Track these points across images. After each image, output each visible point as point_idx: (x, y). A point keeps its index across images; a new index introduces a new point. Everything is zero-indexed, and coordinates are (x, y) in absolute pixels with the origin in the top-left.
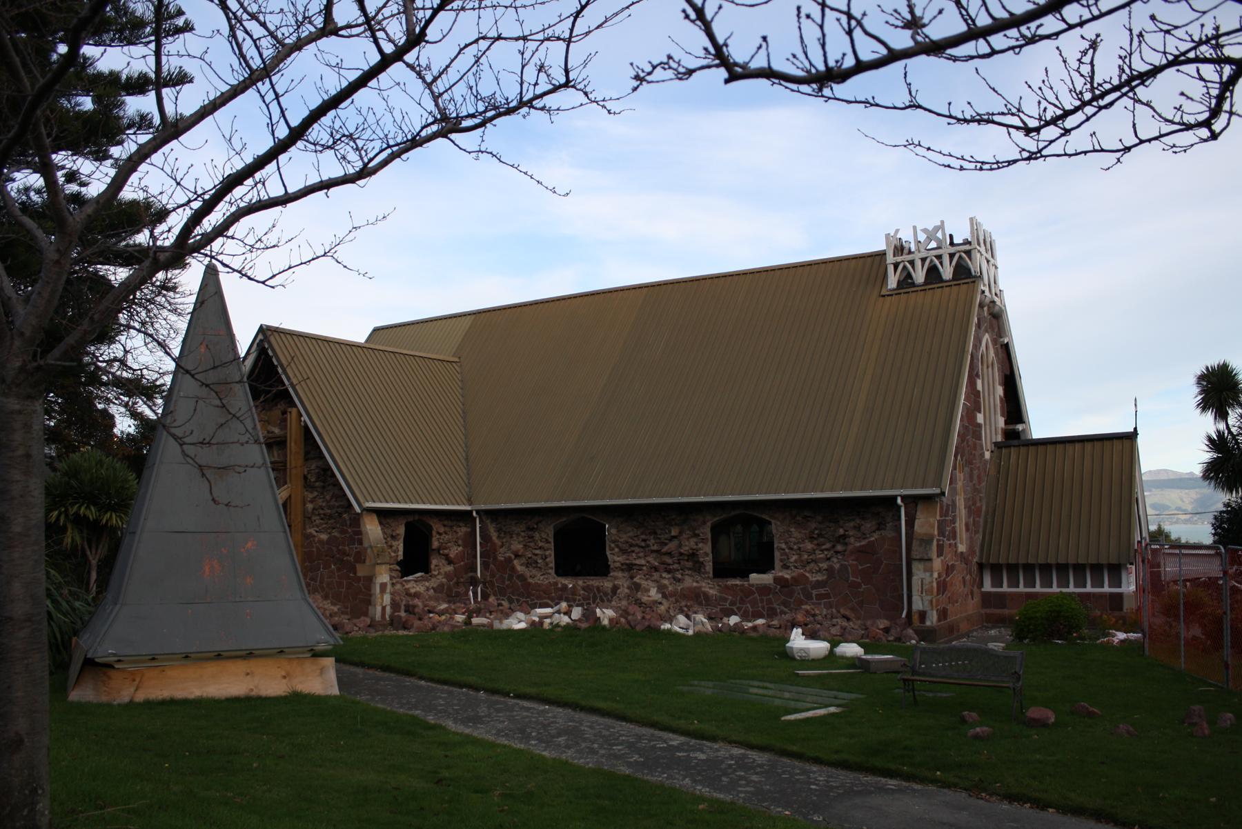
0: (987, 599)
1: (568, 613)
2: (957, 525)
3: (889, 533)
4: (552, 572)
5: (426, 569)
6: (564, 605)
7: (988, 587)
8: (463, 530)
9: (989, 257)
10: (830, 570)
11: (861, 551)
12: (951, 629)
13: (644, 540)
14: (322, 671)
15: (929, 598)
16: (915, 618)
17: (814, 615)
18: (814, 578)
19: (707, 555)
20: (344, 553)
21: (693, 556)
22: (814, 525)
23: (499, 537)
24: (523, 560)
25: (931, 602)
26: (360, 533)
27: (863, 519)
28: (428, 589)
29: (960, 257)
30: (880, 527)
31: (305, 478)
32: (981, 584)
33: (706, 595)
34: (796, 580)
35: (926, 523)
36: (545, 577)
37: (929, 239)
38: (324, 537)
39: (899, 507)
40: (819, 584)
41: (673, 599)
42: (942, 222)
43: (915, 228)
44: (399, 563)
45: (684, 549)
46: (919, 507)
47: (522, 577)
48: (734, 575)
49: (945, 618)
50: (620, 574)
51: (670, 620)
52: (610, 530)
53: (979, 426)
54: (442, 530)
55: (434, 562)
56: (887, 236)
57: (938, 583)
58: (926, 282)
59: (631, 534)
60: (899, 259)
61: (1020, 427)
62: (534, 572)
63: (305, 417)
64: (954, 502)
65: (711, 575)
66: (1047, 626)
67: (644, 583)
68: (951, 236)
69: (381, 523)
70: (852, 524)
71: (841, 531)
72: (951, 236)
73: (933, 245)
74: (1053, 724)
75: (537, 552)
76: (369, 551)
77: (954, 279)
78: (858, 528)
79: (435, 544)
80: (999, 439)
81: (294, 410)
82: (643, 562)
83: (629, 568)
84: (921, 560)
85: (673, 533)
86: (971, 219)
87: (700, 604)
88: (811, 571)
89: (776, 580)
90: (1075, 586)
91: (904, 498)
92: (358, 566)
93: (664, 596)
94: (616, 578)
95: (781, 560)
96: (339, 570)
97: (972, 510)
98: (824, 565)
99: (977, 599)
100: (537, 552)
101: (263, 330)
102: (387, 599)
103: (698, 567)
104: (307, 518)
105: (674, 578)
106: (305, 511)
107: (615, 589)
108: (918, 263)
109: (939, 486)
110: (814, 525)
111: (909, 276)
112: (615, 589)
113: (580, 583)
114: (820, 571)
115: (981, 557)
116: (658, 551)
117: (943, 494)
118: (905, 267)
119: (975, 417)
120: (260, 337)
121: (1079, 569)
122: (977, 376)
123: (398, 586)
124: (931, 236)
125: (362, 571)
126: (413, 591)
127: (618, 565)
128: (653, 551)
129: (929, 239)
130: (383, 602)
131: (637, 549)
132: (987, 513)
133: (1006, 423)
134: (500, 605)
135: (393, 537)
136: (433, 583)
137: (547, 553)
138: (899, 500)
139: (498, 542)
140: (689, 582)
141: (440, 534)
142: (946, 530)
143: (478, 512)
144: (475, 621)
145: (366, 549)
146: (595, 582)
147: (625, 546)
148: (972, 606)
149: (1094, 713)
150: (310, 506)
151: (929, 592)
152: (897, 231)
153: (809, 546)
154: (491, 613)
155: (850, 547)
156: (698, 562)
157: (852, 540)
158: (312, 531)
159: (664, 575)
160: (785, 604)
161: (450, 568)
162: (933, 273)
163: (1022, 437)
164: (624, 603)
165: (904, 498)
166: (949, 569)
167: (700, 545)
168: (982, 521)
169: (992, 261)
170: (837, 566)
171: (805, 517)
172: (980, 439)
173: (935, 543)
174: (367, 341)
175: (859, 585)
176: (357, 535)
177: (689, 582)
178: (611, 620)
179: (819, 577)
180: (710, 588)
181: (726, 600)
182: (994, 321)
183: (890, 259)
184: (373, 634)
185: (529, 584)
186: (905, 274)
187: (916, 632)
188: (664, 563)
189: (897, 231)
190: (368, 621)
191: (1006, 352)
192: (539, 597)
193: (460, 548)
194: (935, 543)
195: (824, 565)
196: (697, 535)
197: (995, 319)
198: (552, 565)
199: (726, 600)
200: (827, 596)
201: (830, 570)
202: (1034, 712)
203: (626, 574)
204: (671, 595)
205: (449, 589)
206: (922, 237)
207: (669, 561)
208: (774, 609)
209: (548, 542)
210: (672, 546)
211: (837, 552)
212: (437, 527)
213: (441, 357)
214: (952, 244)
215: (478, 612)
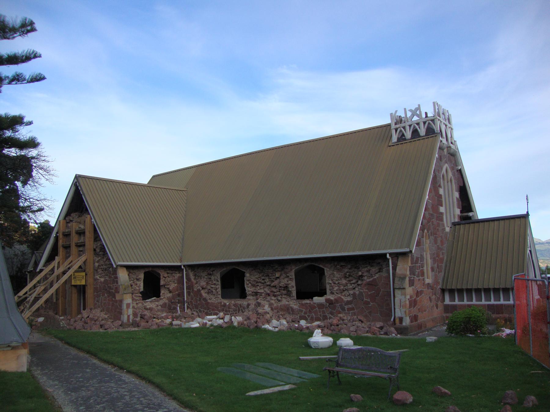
0: (448, 309)
1: (223, 318)
2: (425, 268)
3: (384, 274)
4: (220, 296)
5: (158, 295)
6: (221, 314)
7: (447, 301)
8: (177, 275)
9: (447, 124)
10: (354, 294)
11: (369, 284)
12: (420, 327)
13: (263, 280)
14: (18, 358)
15: (404, 310)
16: (397, 321)
17: (343, 320)
18: (346, 299)
19: (293, 287)
20: (110, 288)
21: (286, 287)
22: (346, 270)
23: (195, 279)
24: (206, 291)
25: (405, 312)
26: (117, 278)
27: (372, 266)
28: (157, 306)
29: (429, 123)
30: (380, 270)
31: (95, 250)
32: (444, 300)
33: (292, 308)
34: (337, 301)
35: (403, 267)
36: (216, 299)
37: (413, 116)
38: (102, 280)
39: (389, 259)
40: (349, 303)
41: (276, 311)
42: (419, 105)
43: (405, 109)
44: (141, 293)
45: (282, 284)
47: (205, 299)
48: (308, 298)
49: (416, 320)
50: (251, 297)
51: (268, 322)
52: (328, 272)
53: (442, 213)
54: (166, 275)
55: (162, 292)
56: (391, 114)
57: (410, 302)
59: (257, 276)
60: (397, 126)
61: (471, 214)
62: (212, 296)
63: (93, 220)
64: (422, 256)
65: (295, 298)
66: (465, 327)
67: (263, 302)
68: (426, 113)
69: (127, 271)
70: (366, 269)
71: (360, 273)
72: (426, 113)
73: (415, 118)
74: (411, 404)
75: (213, 286)
76: (121, 287)
78: (368, 271)
79: (162, 283)
80: (457, 220)
81: (89, 216)
82: (262, 291)
83: (256, 294)
84: (399, 289)
85: (277, 276)
86: (434, 103)
87: (289, 313)
88: (345, 295)
89: (327, 300)
90: (495, 301)
91: (391, 254)
92: (116, 294)
93: (272, 309)
94: (249, 300)
95: (330, 290)
96: (108, 297)
97: (436, 258)
98: (351, 292)
99: (441, 308)
100: (213, 286)
101: (77, 177)
102: (130, 311)
103: (289, 294)
104: (96, 270)
105: (277, 299)
106: (94, 266)
107: (248, 305)
108: (408, 128)
109: (408, 246)
110: (346, 270)
112: (248, 305)
113: (233, 302)
114: (349, 295)
115: (443, 285)
116: (270, 285)
117: (411, 251)
118: (401, 131)
119: (438, 209)
120: (76, 180)
121: (496, 291)
122: (440, 186)
123: (140, 305)
124: (414, 113)
125: (118, 297)
126: (148, 307)
127: (250, 293)
128: (267, 285)
129: (413, 116)
130: (128, 314)
131: (260, 284)
132: (447, 261)
133: (461, 212)
134: (193, 314)
135: (138, 280)
136: (161, 302)
137: (217, 287)
139: (194, 282)
140: (284, 302)
141: (165, 278)
142: (417, 271)
143: (184, 266)
144: (175, 322)
145: (119, 286)
146: (240, 302)
147: (254, 283)
148: (437, 313)
149: (445, 393)
150: (97, 264)
151: (404, 306)
152: (396, 111)
153: (344, 281)
154: (185, 318)
155: (364, 282)
156: (289, 291)
157: (365, 278)
158: (98, 277)
159: (273, 298)
160: (331, 313)
161: (170, 295)
162: (415, 133)
163: (473, 219)
164: (250, 313)
165: (390, 254)
166: (418, 294)
167: (290, 282)
168: (444, 265)
169: (449, 125)
170: (357, 293)
171: (341, 266)
172: (442, 220)
173: (407, 279)
174: (148, 183)
175: (369, 303)
176: (115, 279)
177: (284, 302)
178: (239, 323)
179: (349, 299)
180: (294, 304)
181: (302, 311)
182: (452, 158)
183: (393, 126)
184: (121, 329)
185: (208, 303)
186: (401, 134)
187: (396, 329)
188: (272, 292)
189: (396, 111)
190: (120, 323)
191: (460, 174)
192: (213, 310)
193: (176, 285)
194: (407, 279)
195: (351, 292)
196: (288, 277)
197: (452, 157)
198: (220, 293)
199: (302, 311)
200: (353, 309)
201: (354, 294)
202: (399, 395)
203: (255, 297)
204: (275, 309)
205: (170, 306)
206: (409, 114)
207: (274, 290)
208: (326, 316)
209: (218, 281)
210: (276, 283)
211: (358, 285)
212: (163, 274)
213: (177, 189)
214: (426, 116)
215: (177, 318)
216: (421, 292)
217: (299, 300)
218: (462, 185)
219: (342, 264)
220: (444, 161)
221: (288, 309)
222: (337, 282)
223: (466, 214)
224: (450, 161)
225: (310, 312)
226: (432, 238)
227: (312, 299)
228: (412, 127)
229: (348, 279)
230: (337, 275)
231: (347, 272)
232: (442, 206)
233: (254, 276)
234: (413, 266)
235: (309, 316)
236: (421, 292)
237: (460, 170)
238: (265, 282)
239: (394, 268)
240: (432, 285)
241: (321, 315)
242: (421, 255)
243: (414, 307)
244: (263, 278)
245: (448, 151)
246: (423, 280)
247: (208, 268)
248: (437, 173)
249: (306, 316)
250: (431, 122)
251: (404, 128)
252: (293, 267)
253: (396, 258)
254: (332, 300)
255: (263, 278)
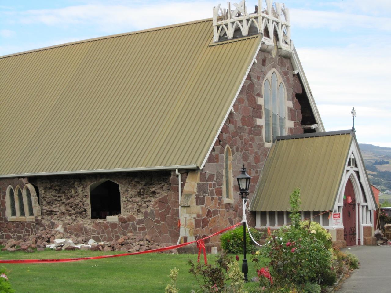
13: (59, 197)
40: (140, 222)
46: (189, 175)
52: (122, 189)
58: (234, 37)
60: (220, 23)
61: (313, 126)
65: (90, 217)
67: (56, 222)
70: (159, 186)
77: (249, 35)
82: (57, 209)
87: (83, 234)
108: (230, 25)
110: (141, 187)
111: (225, 34)
131: (56, 202)
138: (177, 172)
153: (138, 199)
162: (237, 31)
180: (88, 223)
183: (215, 23)
200: (143, 229)
216: (216, 212)
217: (94, 220)
218: (301, 92)
219: (136, 180)
220: (268, 64)
221: (81, 229)
222: (131, 200)
223: (307, 126)
224: (282, 64)
225: (103, 232)
226: (239, 154)
227: (105, 218)
228: (235, 24)
229: (142, 197)
230: (132, 192)
231: (141, 189)
232: (260, 117)
233: (49, 193)
234: (203, 184)
235: (101, 237)
236: (216, 212)
237: (298, 74)
238: (61, 200)
239: (183, 186)
240: (234, 206)
241: (113, 236)
242: (218, 172)
243: (203, 227)
244: (59, 195)
245: (278, 52)
246: (220, 199)
247: (62, 183)
248: (255, 80)
249: (99, 236)
250: (254, 20)
251: (226, 25)
252: (89, 183)
253: (185, 175)
254: (124, 219)
255: (59, 195)
